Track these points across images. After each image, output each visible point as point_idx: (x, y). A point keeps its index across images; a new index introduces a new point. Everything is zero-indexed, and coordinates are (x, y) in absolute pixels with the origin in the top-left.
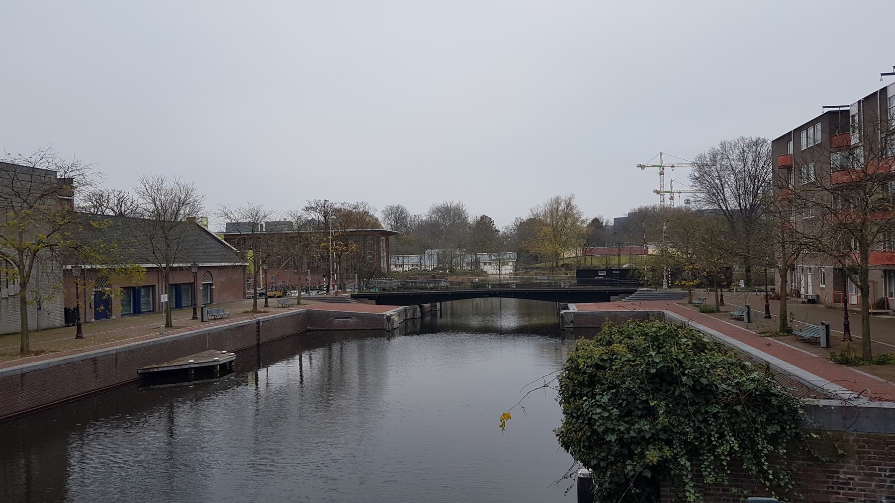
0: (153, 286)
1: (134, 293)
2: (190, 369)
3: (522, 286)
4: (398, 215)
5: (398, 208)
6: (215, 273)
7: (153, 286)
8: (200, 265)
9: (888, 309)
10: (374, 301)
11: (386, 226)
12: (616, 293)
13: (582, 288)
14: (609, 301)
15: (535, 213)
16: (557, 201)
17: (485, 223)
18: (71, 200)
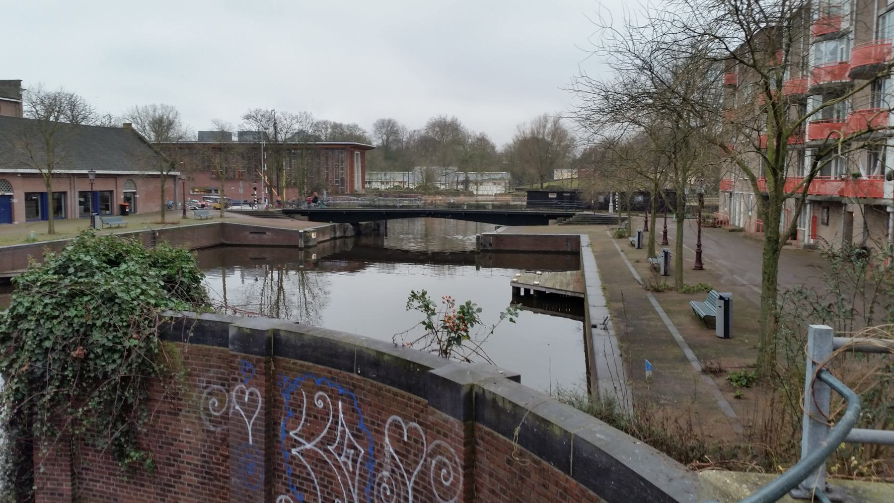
0: (65, 193)
1: (42, 198)
2: (582, 318)
3: (500, 207)
4: (389, 128)
5: (389, 121)
6: (139, 182)
7: (65, 193)
8: (98, 172)
9: (43, 195)
10: (306, 217)
11: (376, 142)
12: (554, 217)
13: (529, 211)
14: (547, 224)
15: (521, 130)
16: (546, 119)
17: (483, 143)
18: (18, 103)
